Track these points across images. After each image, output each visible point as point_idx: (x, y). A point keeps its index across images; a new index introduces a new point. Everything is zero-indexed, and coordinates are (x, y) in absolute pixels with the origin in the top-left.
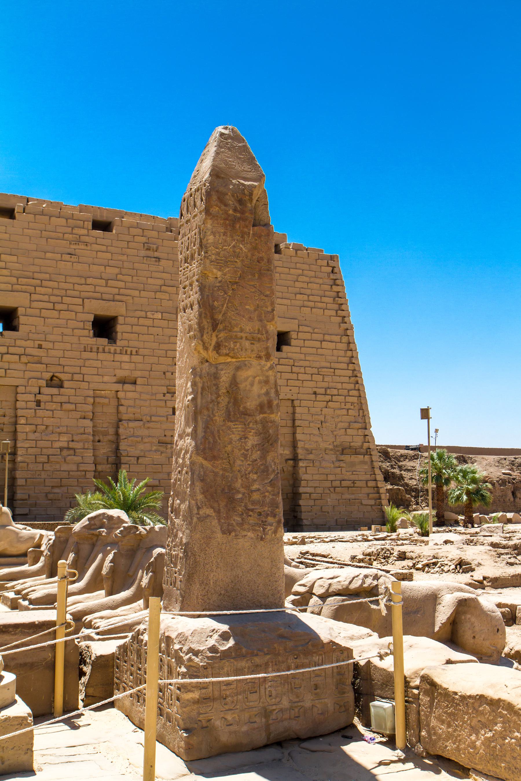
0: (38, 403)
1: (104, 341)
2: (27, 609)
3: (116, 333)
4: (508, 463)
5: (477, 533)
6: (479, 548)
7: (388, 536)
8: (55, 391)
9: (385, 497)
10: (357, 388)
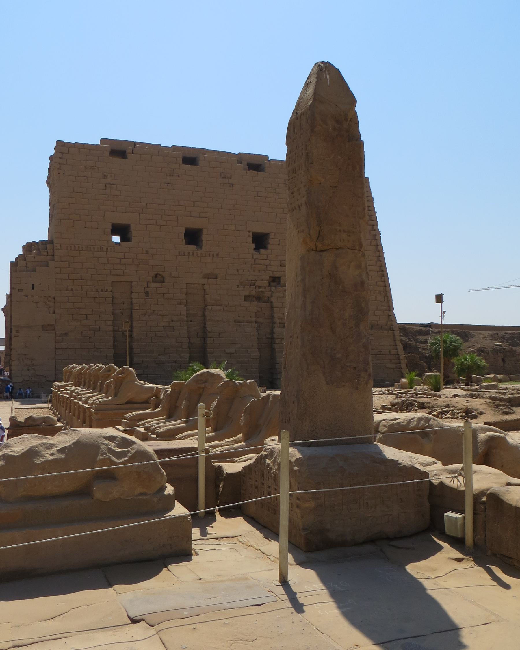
0: (147, 294)
1: (192, 247)
2: (154, 440)
3: (202, 241)
4: (499, 337)
5: (476, 389)
6: (482, 400)
7: (409, 391)
8: (158, 285)
9: (404, 361)
10: (383, 280)
